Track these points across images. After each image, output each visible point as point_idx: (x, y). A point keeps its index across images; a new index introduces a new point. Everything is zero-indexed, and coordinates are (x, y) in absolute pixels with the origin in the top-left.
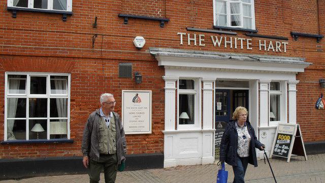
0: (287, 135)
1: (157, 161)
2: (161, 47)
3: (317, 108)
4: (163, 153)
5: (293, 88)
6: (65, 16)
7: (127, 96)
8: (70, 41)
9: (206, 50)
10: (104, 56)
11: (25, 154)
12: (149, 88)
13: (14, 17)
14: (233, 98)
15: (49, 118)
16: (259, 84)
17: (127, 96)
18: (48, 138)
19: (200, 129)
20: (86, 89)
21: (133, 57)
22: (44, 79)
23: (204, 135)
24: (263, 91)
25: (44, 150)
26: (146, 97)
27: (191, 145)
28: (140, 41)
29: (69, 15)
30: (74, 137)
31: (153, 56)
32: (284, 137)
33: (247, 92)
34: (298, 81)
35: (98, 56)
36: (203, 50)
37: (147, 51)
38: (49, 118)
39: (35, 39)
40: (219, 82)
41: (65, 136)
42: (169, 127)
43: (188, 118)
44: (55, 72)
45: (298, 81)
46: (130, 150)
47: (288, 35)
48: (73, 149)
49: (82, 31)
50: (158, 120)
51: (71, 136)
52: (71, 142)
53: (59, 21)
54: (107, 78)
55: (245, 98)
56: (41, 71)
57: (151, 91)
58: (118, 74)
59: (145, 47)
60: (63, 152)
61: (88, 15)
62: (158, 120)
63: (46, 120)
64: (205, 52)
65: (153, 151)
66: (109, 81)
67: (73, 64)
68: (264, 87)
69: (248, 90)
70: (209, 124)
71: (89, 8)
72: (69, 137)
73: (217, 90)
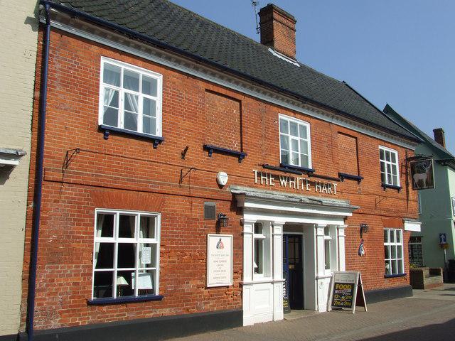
0: (347, 284)
1: (235, 317)
2: (240, 185)
3: (360, 254)
4: (242, 307)
5: (342, 233)
6: (155, 142)
7: (213, 240)
8: (160, 173)
9: (275, 190)
10: (193, 194)
11: (113, 316)
12: (230, 232)
13: (105, 139)
14: (296, 241)
15: (116, 269)
16: (273, 226)
17: (213, 240)
18: (137, 295)
19: (270, 279)
20: (175, 233)
21: (215, 196)
22: (133, 217)
23: (275, 284)
24: (277, 235)
25: (133, 310)
26: (228, 240)
27: (263, 302)
28: (223, 178)
29: (160, 141)
30: (161, 292)
31: (234, 195)
32: (343, 287)
33: (300, 237)
34: (346, 226)
35: (186, 192)
36: (273, 190)
37: (228, 189)
38: (116, 269)
39: (127, 168)
40: (287, 227)
41: (152, 291)
42: (247, 279)
43: (126, 283)
44: (146, 210)
45: (346, 226)
46: (214, 306)
47: (337, 177)
48: (162, 307)
49: (172, 162)
50: (238, 271)
51: (160, 290)
52: (159, 298)
53: (149, 145)
54: (193, 219)
55: (297, 245)
56: (131, 208)
57: (232, 235)
58: (204, 215)
59: (227, 185)
60: (151, 312)
61: (176, 143)
62: (238, 271)
63: (112, 272)
64: (275, 192)
65: (233, 307)
66: (195, 223)
67: (163, 200)
68: (321, 232)
69: (300, 237)
70: (279, 275)
71: (177, 134)
72: (157, 293)
73: (284, 235)
